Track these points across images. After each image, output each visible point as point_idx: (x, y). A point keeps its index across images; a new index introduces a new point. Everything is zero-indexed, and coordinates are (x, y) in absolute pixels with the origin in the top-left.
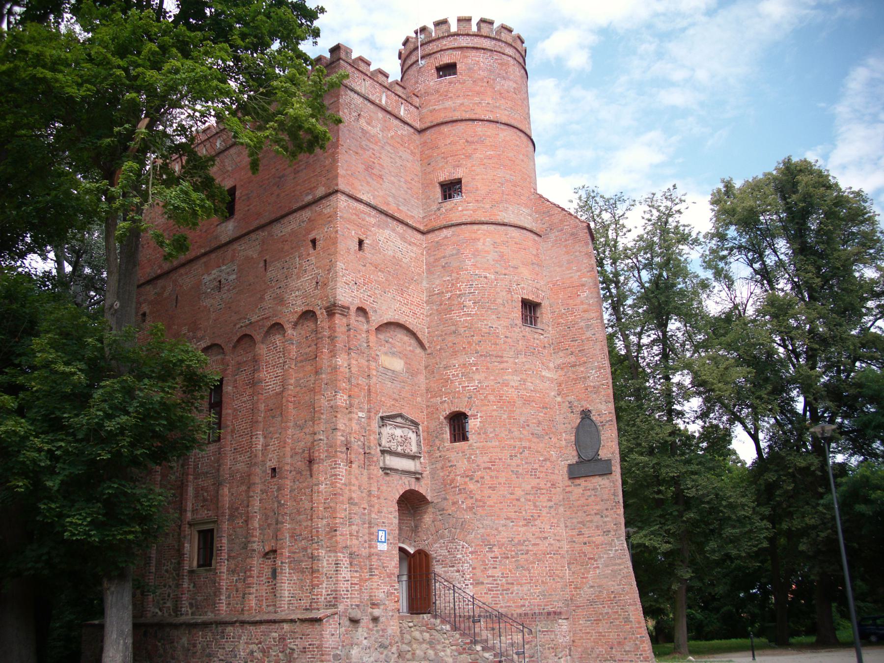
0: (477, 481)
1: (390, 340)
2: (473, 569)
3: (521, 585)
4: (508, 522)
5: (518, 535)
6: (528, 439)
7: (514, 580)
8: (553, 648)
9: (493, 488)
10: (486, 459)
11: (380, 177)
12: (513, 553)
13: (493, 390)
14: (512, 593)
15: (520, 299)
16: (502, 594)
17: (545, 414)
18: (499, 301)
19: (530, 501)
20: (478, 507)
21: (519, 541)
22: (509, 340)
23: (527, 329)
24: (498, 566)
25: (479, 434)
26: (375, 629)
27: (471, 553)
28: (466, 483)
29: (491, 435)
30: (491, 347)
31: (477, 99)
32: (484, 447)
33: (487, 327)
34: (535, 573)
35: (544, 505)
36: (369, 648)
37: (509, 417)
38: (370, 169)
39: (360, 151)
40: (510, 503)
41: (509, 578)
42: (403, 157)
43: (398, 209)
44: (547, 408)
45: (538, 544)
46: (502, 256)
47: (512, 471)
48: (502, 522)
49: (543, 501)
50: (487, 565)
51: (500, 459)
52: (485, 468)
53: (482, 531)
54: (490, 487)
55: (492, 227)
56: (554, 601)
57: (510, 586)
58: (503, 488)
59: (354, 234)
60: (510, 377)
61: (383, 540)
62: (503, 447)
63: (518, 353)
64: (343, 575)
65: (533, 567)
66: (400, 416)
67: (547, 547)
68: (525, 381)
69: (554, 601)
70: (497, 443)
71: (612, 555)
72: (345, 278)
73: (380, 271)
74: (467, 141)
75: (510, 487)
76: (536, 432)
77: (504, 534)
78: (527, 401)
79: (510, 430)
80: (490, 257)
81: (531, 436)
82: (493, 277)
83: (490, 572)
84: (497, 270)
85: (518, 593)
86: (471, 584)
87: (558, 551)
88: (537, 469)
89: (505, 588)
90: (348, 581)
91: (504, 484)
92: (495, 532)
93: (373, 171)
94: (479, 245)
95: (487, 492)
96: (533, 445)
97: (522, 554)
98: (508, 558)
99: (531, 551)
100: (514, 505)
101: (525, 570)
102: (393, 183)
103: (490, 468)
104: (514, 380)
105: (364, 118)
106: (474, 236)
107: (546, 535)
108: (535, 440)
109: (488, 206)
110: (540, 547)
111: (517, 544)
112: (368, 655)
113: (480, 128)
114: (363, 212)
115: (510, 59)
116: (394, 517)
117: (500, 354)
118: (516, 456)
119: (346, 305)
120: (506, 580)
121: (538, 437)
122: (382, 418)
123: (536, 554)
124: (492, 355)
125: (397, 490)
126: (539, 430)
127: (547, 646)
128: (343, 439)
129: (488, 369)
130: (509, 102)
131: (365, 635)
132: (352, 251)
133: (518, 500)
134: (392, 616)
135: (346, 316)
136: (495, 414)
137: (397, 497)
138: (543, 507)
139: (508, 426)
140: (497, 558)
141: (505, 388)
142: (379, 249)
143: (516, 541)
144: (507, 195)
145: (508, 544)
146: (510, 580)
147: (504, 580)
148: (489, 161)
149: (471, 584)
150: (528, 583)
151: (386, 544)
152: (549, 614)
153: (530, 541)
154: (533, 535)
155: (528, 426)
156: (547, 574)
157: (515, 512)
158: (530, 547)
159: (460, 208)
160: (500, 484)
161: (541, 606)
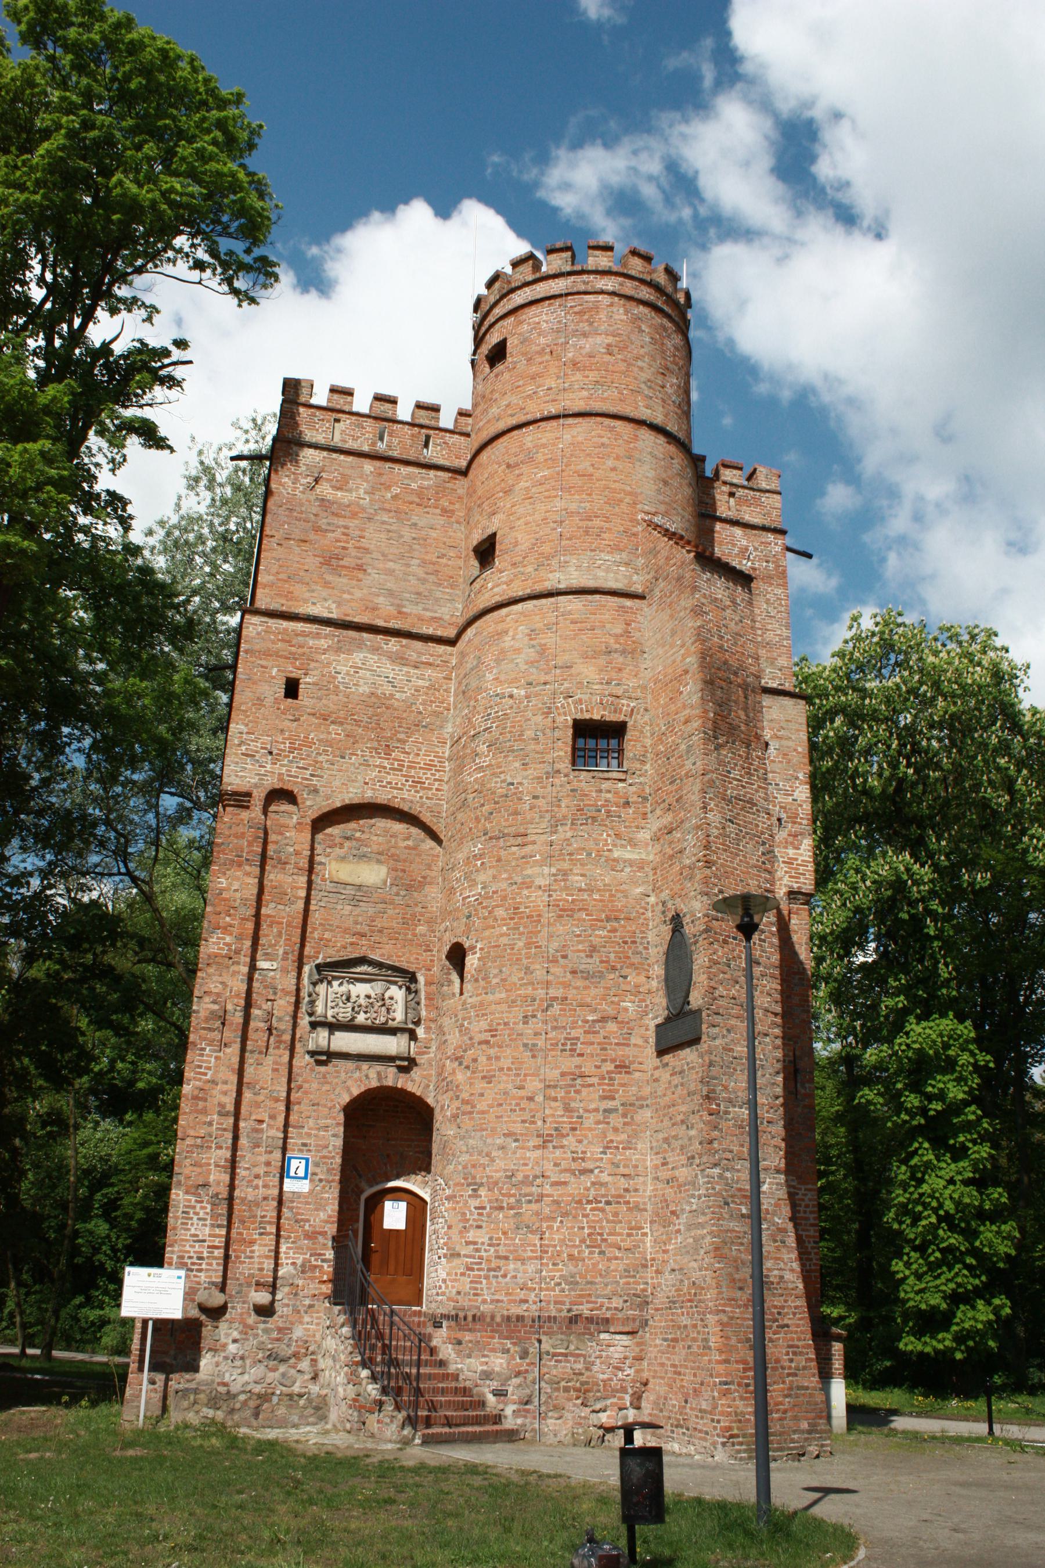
0: (467, 1067)
1: (358, 834)
2: (449, 1227)
3: (523, 1261)
4: (509, 1140)
5: (526, 1165)
6: (563, 983)
7: (510, 1252)
8: (578, 1390)
9: (488, 1079)
10: (484, 1025)
11: (360, 568)
12: (512, 1200)
13: (504, 898)
14: (505, 1276)
15: (570, 723)
16: (487, 1277)
17: (614, 930)
18: (529, 734)
19: (555, 1099)
20: (464, 1114)
21: (526, 1177)
22: (541, 802)
23: (583, 775)
24: (484, 1224)
25: (477, 980)
26: (262, 1326)
27: (448, 1198)
28: (454, 1070)
29: (494, 981)
30: (507, 820)
31: (530, 389)
32: (481, 1004)
33: (504, 785)
34: (553, 1239)
35: (593, 1106)
36: (242, 1358)
37: (528, 945)
38: (334, 562)
39: (312, 536)
40: (517, 1104)
41: (501, 1248)
42: (421, 524)
43: (400, 612)
44: (617, 919)
45: (565, 1183)
46: (543, 650)
47: (525, 1045)
48: (498, 1141)
49: (590, 1098)
50: (468, 1220)
51: (506, 1024)
52: (480, 1043)
53: (464, 1158)
54: (484, 1077)
55: (530, 604)
56: (598, 1296)
57: (502, 1262)
58: (505, 1078)
59: (276, 675)
60: (537, 870)
61: (301, 1173)
62: (513, 1001)
63: (555, 826)
64: (193, 1231)
65: (550, 1228)
66: (363, 961)
67: (587, 1189)
68: (565, 873)
69: (598, 1296)
70: (503, 995)
71: (694, 1207)
72: (243, 748)
73: (333, 722)
74: (509, 466)
75: (518, 1075)
76: (582, 967)
77: (500, 1164)
78: (566, 912)
79: (527, 968)
80: (520, 659)
81: (569, 976)
82: (523, 693)
83: (471, 1235)
84: (531, 679)
85: (515, 1277)
86: (445, 1256)
87: (620, 1196)
88: (578, 1039)
89: (493, 1265)
90: (204, 1241)
91: (509, 1069)
92: (484, 1161)
93: (341, 563)
94: (507, 642)
95: (480, 1085)
96: (571, 993)
97: (530, 1202)
98: (501, 1208)
99: (548, 1196)
100: (523, 1109)
101: (532, 1232)
102: (391, 572)
103: (487, 1042)
104: (542, 875)
105: (328, 480)
106: (500, 627)
107: (590, 1165)
108: (580, 983)
109: (530, 569)
110: (570, 1189)
111: (522, 1182)
112: (239, 1371)
113: (528, 437)
114: (303, 634)
115: (600, 297)
116: (334, 1135)
117: (522, 830)
118: (534, 1016)
119: (244, 789)
120: (496, 1251)
121: (587, 976)
122: (318, 967)
123: (557, 1202)
124: (508, 835)
125: (348, 1089)
126: (593, 964)
127: (563, 1384)
128: (216, 1007)
129: (499, 860)
130: (591, 374)
131: (235, 1334)
132: (269, 701)
133: (531, 1099)
134: (311, 1306)
135: (248, 807)
136: (504, 940)
137: (346, 1099)
138: (587, 1111)
139: (525, 961)
140: (484, 1208)
141: (525, 892)
142: (337, 687)
143: (520, 1176)
144: (570, 539)
145: (504, 1183)
146: (502, 1250)
147: (492, 1249)
148: (541, 489)
149: (445, 1256)
150: (536, 1258)
151: (307, 1182)
152: (574, 1320)
153: (548, 1177)
154: (556, 1165)
155: (564, 957)
156: (583, 1241)
157: (524, 1121)
158: (548, 1189)
159: (490, 585)
160: (501, 1069)
161: (563, 1303)
